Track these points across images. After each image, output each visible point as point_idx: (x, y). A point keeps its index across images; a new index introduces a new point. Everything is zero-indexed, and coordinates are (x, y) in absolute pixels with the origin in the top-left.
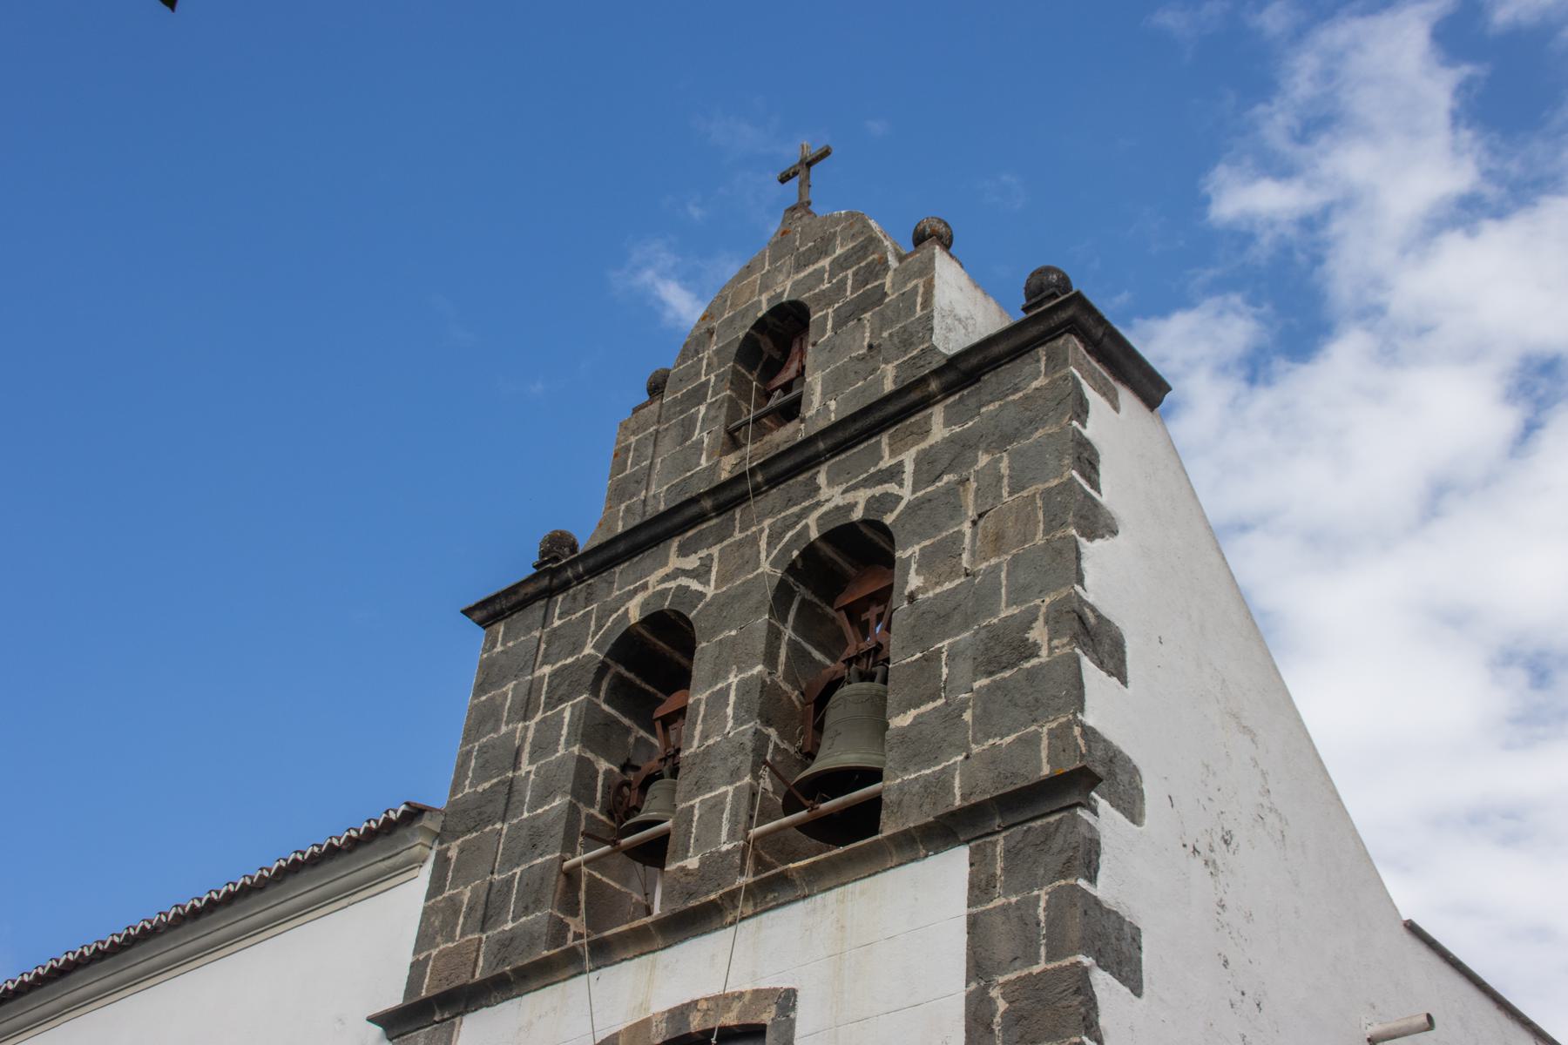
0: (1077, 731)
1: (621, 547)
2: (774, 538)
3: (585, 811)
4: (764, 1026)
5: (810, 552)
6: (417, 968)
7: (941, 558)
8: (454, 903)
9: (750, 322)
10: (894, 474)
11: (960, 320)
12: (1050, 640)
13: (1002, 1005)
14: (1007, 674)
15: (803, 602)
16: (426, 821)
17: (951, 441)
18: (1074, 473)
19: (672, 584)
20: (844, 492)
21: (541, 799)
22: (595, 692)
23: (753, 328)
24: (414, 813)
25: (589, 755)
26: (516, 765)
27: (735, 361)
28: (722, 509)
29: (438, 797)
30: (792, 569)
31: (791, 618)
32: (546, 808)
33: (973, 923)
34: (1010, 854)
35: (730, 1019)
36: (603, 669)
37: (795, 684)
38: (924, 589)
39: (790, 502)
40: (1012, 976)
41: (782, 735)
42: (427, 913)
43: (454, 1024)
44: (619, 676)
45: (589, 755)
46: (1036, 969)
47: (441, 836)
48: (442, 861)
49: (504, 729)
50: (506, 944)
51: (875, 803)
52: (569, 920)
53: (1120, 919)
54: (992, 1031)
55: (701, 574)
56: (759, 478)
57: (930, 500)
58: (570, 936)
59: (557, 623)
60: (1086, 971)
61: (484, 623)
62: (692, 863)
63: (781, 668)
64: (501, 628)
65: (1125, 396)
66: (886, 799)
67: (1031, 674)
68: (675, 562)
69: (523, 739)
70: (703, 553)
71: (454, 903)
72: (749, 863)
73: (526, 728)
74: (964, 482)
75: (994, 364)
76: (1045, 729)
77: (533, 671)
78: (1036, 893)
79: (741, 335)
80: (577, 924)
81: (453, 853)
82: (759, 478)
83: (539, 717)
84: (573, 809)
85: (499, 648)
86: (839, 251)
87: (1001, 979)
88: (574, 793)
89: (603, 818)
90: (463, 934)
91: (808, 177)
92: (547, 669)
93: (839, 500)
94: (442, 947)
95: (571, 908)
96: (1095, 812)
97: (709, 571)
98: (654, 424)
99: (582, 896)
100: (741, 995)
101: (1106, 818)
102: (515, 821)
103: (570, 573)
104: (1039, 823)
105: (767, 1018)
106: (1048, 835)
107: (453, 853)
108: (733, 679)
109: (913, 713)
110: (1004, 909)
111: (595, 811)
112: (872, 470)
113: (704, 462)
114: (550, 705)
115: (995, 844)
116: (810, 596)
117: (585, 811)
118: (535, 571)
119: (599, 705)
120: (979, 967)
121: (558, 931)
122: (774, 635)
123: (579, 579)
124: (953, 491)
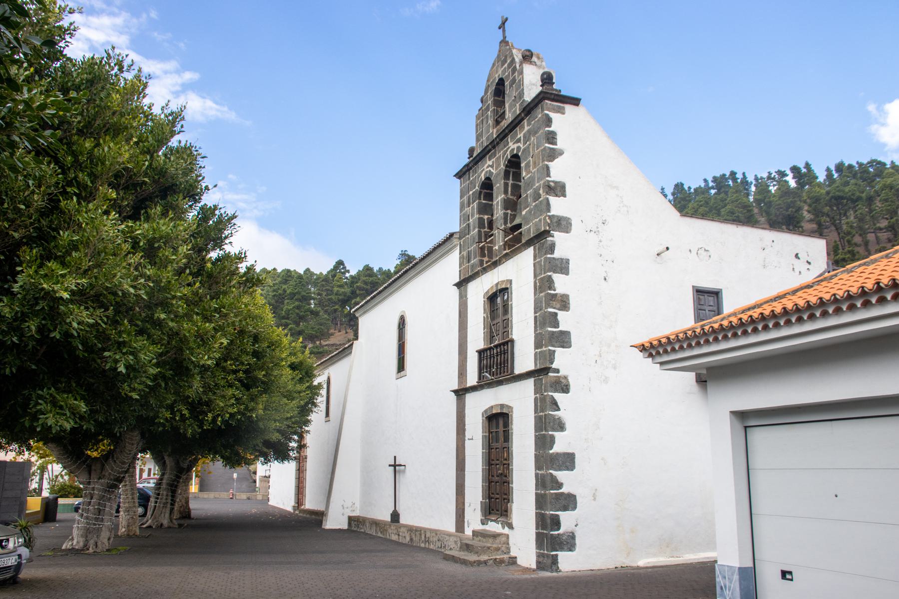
0: (547, 218)
1: (478, 158)
2: (503, 156)
3: (482, 230)
5: (509, 161)
6: (460, 271)
7: (528, 165)
8: (463, 255)
9: (495, 84)
10: (519, 141)
11: (534, 85)
13: (538, 284)
14: (537, 202)
15: (513, 172)
16: (455, 236)
17: (529, 131)
18: (547, 145)
19: (488, 169)
21: (474, 229)
22: (480, 199)
24: (452, 235)
25: (482, 216)
26: (469, 220)
28: (494, 147)
29: (456, 229)
30: (507, 166)
31: (511, 178)
34: (539, 249)
35: (490, 293)
36: (480, 193)
37: (514, 196)
38: (525, 176)
39: (505, 147)
41: (512, 211)
42: (460, 258)
44: (485, 192)
45: (482, 216)
46: (542, 276)
47: (460, 238)
48: (460, 245)
50: (472, 266)
51: (521, 233)
52: (483, 259)
53: (562, 259)
55: (492, 166)
56: (498, 140)
58: (485, 262)
59: (471, 179)
60: (550, 276)
61: (460, 178)
62: (497, 247)
63: (509, 193)
64: (462, 179)
65: (568, 108)
66: (523, 233)
67: (541, 202)
70: (492, 160)
71: (463, 255)
72: (507, 247)
74: (530, 144)
75: (536, 105)
81: (462, 243)
82: (498, 140)
84: (479, 232)
86: (508, 61)
88: (479, 227)
91: (504, 28)
92: (471, 193)
93: (512, 147)
95: (483, 255)
96: (553, 237)
99: (486, 252)
100: (504, 281)
101: (558, 237)
103: (470, 165)
105: (508, 286)
106: (543, 244)
107: (462, 243)
108: (499, 198)
109: (525, 211)
110: (538, 262)
113: (491, 131)
114: (473, 203)
116: (514, 170)
117: (482, 230)
118: (468, 160)
120: (535, 276)
121: (481, 262)
122: (506, 185)
123: (473, 166)
124: (528, 147)
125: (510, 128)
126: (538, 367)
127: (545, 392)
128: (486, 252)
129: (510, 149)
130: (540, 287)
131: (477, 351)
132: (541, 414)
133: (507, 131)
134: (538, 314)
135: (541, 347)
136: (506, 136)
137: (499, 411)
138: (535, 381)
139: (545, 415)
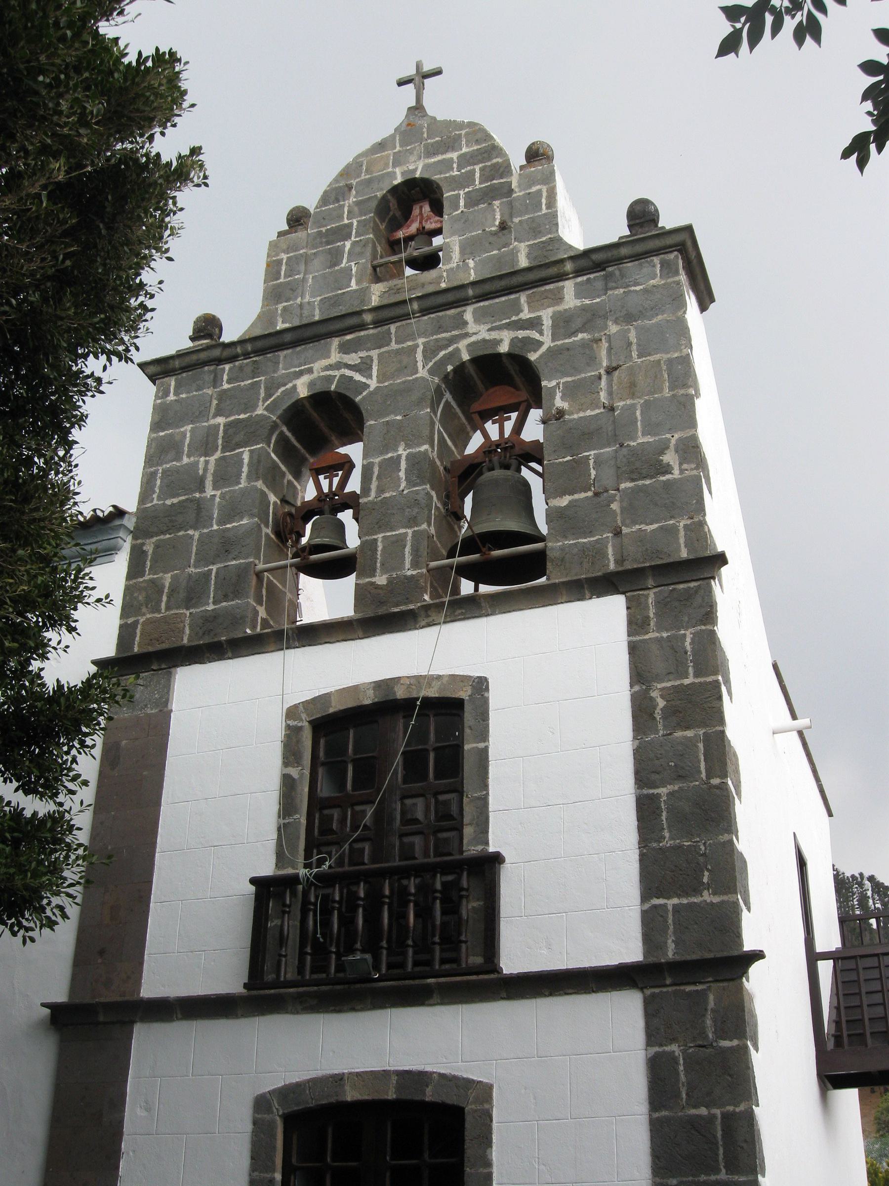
4: (463, 700)
5: (460, 369)
12: (681, 464)
14: (648, 482)
20: (489, 330)
23: (389, 191)
25: (266, 489)
27: (375, 213)
32: (235, 524)
33: (633, 649)
36: (275, 426)
39: (440, 329)
40: (669, 684)
43: (170, 673)
44: (282, 433)
45: (266, 489)
46: (686, 682)
49: (185, 460)
52: (259, 608)
54: (655, 718)
57: (568, 349)
61: (153, 378)
68: (335, 357)
69: (206, 470)
73: (207, 462)
76: (682, 524)
77: (208, 420)
78: (683, 632)
79: (379, 194)
80: (262, 612)
83: (218, 454)
85: (172, 397)
87: (659, 686)
89: (273, 536)
90: (168, 608)
94: (148, 616)
97: (370, 368)
98: (303, 248)
102: (205, 531)
104: (681, 586)
105: (464, 694)
106: (689, 596)
107: (149, 548)
111: (269, 531)
112: (514, 318)
115: (647, 596)
119: (269, 454)
123: (246, 355)
125: (260, 344)
126: (671, 952)
127: (722, 1034)
128: (264, 592)
129: (473, 339)
130: (669, 712)
131: (254, 881)
132: (703, 1111)
133: (470, 292)
134: (663, 791)
135: (697, 891)
136: (463, 302)
137: (391, 1095)
138: (648, 1003)
139: (726, 1116)
